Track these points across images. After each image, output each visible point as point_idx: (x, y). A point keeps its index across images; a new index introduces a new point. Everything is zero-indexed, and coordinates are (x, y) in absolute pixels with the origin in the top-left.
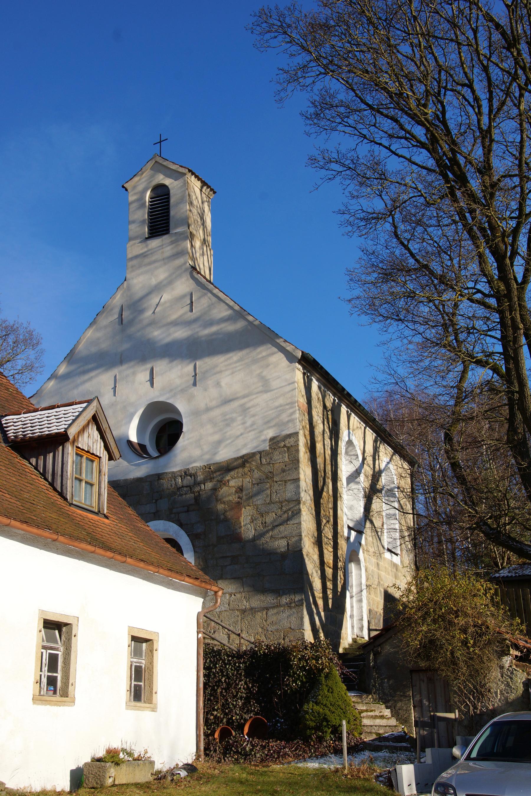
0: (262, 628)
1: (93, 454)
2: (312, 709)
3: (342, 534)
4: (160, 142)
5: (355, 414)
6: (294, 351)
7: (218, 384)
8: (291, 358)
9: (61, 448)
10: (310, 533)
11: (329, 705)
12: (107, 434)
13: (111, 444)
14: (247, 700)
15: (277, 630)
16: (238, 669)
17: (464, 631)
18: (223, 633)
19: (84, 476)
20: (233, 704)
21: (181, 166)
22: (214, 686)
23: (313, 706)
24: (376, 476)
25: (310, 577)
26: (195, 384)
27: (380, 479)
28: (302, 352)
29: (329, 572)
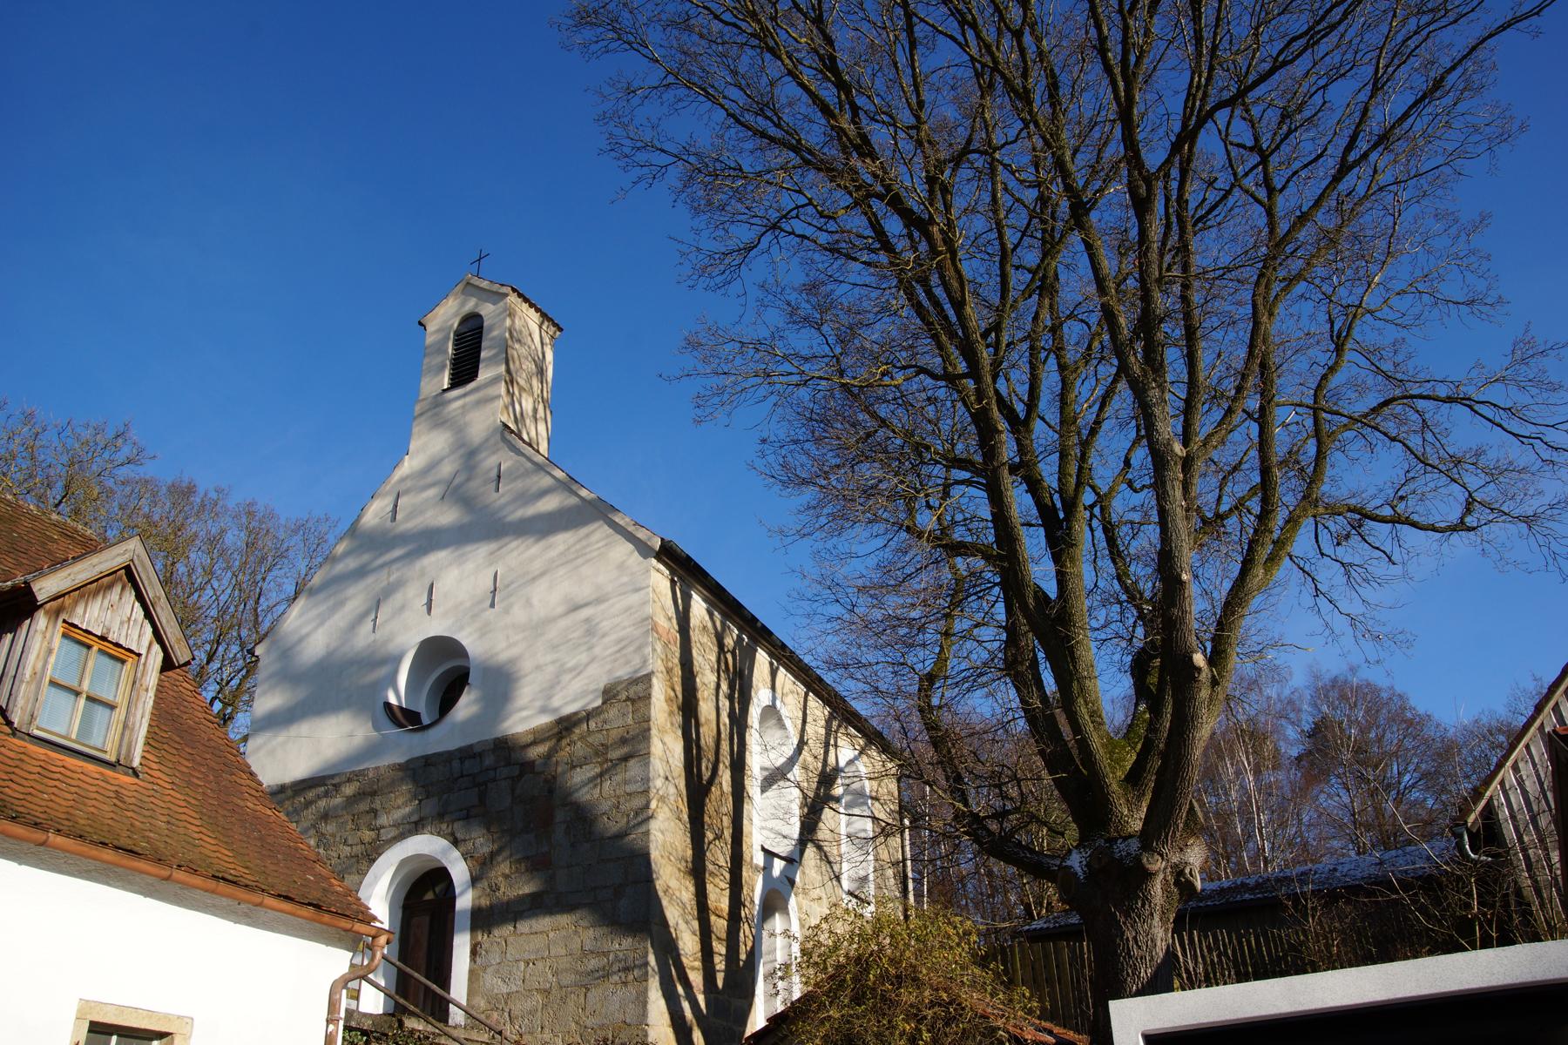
1: (117, 645)
3: (748, 860)
4: (480, 258)
5: (787, 670)
6: (649, 539)
7: (528, 603)
8: (643, 549)
9: (28, 621)
10: (674, 854)
12: (158, 609)
13: (169, 631)
17: (915, 1016)
19: (86, 686)
21: (502, 285)
24: (827, 778)
25: (672, 930)
26: (492, 605)
27: (506, 540)
28: (662, 539)
29: (720, 925)
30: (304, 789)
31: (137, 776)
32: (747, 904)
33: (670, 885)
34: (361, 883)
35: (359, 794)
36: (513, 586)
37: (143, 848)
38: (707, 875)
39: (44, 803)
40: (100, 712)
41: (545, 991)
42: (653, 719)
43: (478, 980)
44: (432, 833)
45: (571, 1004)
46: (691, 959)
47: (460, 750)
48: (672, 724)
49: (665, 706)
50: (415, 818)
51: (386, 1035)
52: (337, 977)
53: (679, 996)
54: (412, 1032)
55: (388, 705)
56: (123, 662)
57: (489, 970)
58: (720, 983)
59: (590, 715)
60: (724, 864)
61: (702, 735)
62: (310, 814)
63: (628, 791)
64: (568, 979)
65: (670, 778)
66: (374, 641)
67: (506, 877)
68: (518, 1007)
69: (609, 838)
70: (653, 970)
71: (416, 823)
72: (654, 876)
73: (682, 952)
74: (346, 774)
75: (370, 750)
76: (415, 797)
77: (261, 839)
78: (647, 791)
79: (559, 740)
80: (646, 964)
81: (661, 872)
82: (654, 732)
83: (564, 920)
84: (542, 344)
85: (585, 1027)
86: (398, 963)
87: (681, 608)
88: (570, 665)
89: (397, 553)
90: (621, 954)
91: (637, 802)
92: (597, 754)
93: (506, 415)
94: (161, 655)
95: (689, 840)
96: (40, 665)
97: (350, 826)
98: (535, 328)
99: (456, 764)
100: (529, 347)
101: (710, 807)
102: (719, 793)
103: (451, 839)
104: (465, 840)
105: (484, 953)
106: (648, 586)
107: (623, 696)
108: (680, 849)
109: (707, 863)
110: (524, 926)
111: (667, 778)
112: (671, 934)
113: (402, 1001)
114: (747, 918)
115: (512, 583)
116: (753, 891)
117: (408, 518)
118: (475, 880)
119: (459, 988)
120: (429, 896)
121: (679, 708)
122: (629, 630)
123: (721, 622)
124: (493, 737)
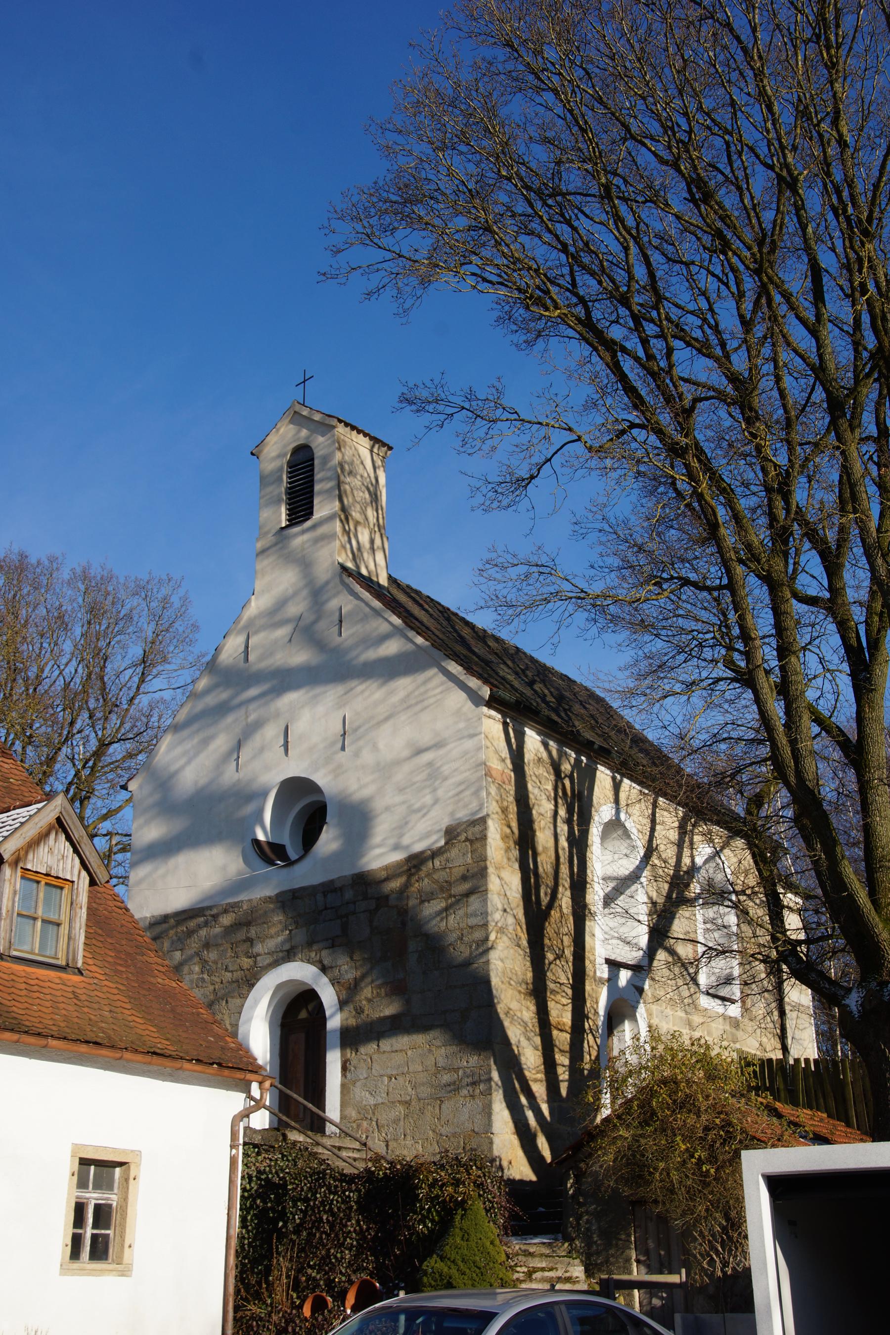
0: (434, 1131)
1: (57, 878)
2: (432, 1268)
3: (591, 974)
4: (304, 382)
6: (480, 689)
7: (375, 748)
10: (514, 977)
11: (460, 1263)
12: (83, 845)
13: (91, 860)
14: (360, 1251)
15: (454, 1135)
16: (346, 1201)
18: (379, 1140)
19: (40, 912)
20: (336, 1257)
22: (311, 1228)
23: (436, 1262)
29: (562, 1039)
30: (185, 920)
31: (82, 974)
32: (590, 1015)
33: (512, 1006)
34: (243, 1005)
35: (236, 924)
36: (362, 730)
37: (102, 1038)
38: (548, 994)
39: (36, 1014)
40: (52, 929)
41: (406, 1102)
42: (489, 858)
43: (349, 1092)
44: (302, 961)
45: (428, 1115)
46: (534, 1072)
47: (323, 885)
48: (509, 859)
49: (501, 844)
50: (287, 947)
51: (273, 1147)
52: (236, 1113)
53: (522, 1106)
54: (295, 1143)
55: (256, 842)
56: (62, 888)
57: (358, 1084)
58: (564, 1092)
59: (436, 853)
60: (566, 982)
61: (539, 864)
62: (194, 944)
63: (470, 924)
64: (425, 1091)
65: (508, 910)
66: (239, 780)
67: (369, 1000)
68: (385, 1117)
69: (455, 967)
70: (497, 1085)
71: (288, 951)
72: (496, 1001)
73: (524, 1066)
74: (222, 905)
75: (241, 885)
76: (286, 928)
77: (173, 1010)
78: (485, 925)
79: (410, 876)
80: (490, 1079)
81: (503, 997)
82: (491, 870)
83: (419, 1039)
84: (375, 468)
85: (441, 1135)
86: (280, 1086)
87: (514, 746)
88: (417, 806)
89: (253, 692)
90: (468, 1071)
91: (478, 935)
92: (442, 889)
93: (344, 555)
94: (88, 879)
95: (528, 964)
96: (10, 904)
97: (229, 953)
98: (365, 453)
99: (320, 897)
100: (362, 476)
101: (549, 930)
102: (558, 915)
103: (320, 965)
104: (331, 967)
105: (352, 1069)
106: (481, 733)
107: (463, 837)
108: (519, 973)
109: (548, 983)
110: (386, 1044)
111: (505, 911)
112: (513, 1051)
113: (284, 1118)
114: (591, 1029)
115: (359, 727)
116: (597, 1003)
117: (262, 658)
118: (342, 1004)
119: (333, 1108)
120: (303, 1015)
121: (515, 843)
122: (467, 774)
123: (558, 750)
124: (352, 872)
